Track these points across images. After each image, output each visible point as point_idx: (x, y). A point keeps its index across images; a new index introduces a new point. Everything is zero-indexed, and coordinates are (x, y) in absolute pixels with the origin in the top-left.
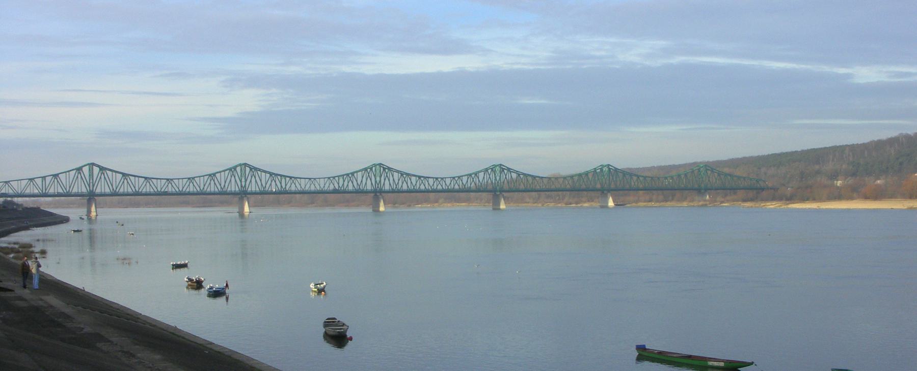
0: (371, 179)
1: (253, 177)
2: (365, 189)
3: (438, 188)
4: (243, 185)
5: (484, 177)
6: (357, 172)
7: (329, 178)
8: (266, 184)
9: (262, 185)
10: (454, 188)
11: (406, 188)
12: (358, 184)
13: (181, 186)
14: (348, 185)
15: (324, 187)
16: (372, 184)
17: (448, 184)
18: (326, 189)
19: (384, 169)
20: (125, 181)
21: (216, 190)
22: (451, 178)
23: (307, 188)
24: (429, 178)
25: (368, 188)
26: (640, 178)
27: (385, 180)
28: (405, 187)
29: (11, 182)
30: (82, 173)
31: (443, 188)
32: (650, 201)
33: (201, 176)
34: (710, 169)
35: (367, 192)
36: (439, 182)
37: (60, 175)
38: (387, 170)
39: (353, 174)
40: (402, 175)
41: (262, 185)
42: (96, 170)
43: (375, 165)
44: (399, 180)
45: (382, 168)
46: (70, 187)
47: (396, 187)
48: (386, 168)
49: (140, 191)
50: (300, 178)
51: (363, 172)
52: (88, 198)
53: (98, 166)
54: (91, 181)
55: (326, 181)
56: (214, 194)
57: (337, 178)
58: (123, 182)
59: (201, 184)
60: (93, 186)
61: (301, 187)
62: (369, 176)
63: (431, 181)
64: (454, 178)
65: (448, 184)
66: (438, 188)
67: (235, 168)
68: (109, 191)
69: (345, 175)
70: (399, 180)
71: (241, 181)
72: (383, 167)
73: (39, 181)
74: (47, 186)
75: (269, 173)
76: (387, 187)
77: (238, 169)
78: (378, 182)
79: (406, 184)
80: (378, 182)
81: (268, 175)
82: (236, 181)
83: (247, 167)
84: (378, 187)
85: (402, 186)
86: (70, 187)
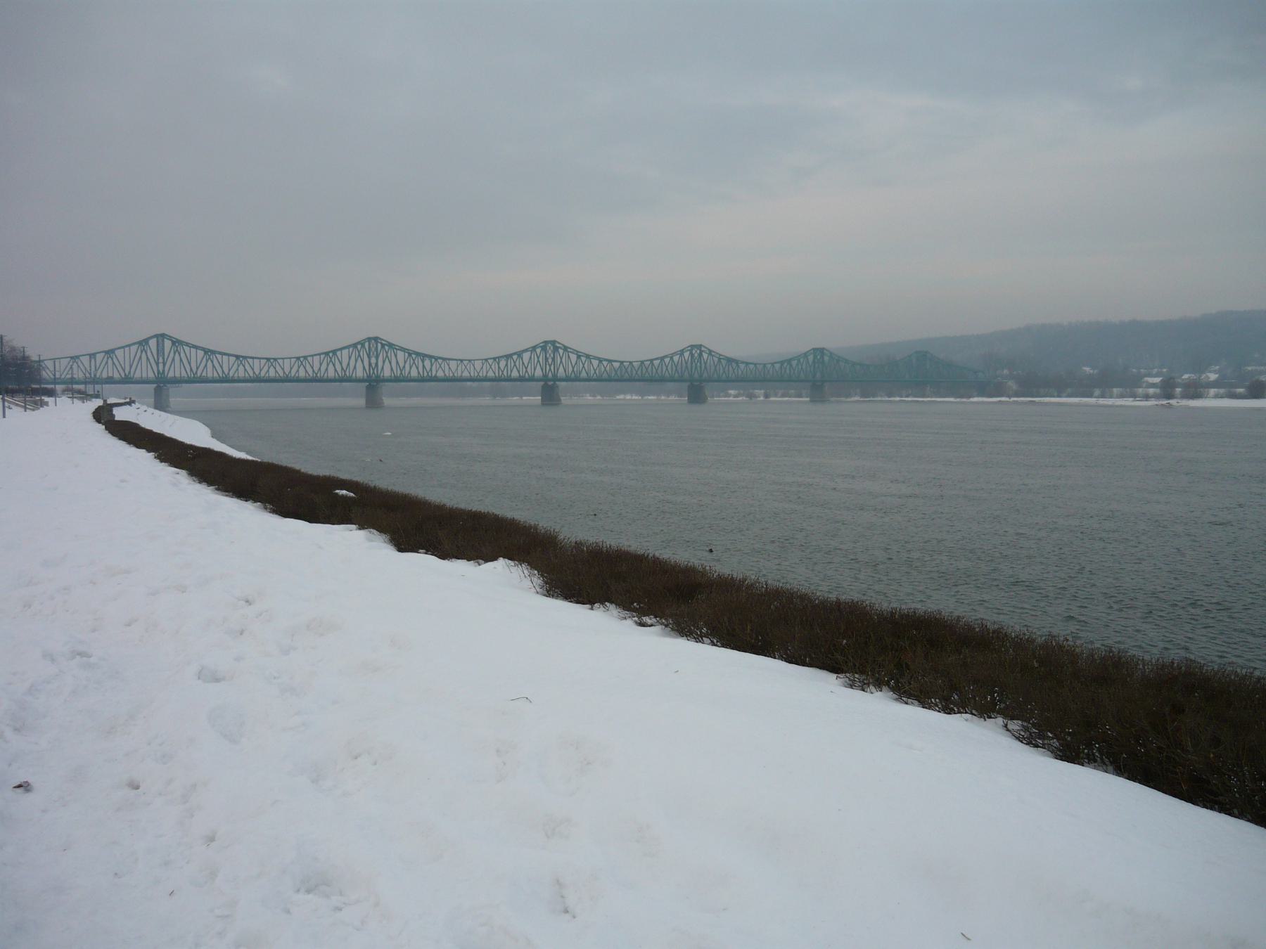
0: (362, 361)
1: (177, 353)
2: (354, 375)
3: (464, 375)
4: (161, 371)
5: (531, 357)
6: (341, 349)
7: (298, 358)
8: (197, 368)
9: (191, 370)
10: (486, 376)
11: (417, 375)
12: (342, 368)
13: (287, 368)
14: (327, 369)
15: (290, 372)
16: (364, 368)
17: (478, 369)
18: (293, 375)
19: (383, 346)
20: (110, 361)
21: (216, 375)
22: (482, 360)
23: (262, 374)
24: (449, 359)
25: (240, 375)
26: (604, 362)
27: (384, 362)
28: (414, 373)
29: (81, 358)
30: (149, 351)
31: (445, 375)
32: (800, 396)
33: (315, 355)
34: (708, 352)
35: (532, 379)
36: (241, 361)
37: (116, 352)
38: (387, 348)
39: (334, 352)
40: (410, 355)
41: (191, 370)
42: (168, 344)
43: (369, 339)
44: (405, 362)
45: (379, 345)
46: (131, 367)
47: (401, 373)
48: (385, 344)
49: (63, 377)
50: (253, 358)
51: (351, 349)
52: (155, 385)
53: (170, 338)
54: (161, 360)
55: (322, 358)
56: (214, 381)
57: (309, 359)
58: (107, 363)
59: (317, 366)
60: (164, 364)
61: (284, 372)
62: (387, 356)
63: (453, 364)
64: (486, 360)
65: (478, 369)
66: (536, 375)
67: (146, 341)
68: (217, 376)
69: (323, 354)
70: (405, 362)
71: (157, 364)
72: (381, 343)
73: (85, 360)
74: (98, 365)
75: (203, 349)
76: (387, 373)
77: (153, 343)
78: (374, 366)
79: (303, 368)
80: (374, 366)
81: (201, 353)
82: (181, 360)
83: (165, 340)
84: (374, 373)
85: (410, 373)
86: (131, 367)
